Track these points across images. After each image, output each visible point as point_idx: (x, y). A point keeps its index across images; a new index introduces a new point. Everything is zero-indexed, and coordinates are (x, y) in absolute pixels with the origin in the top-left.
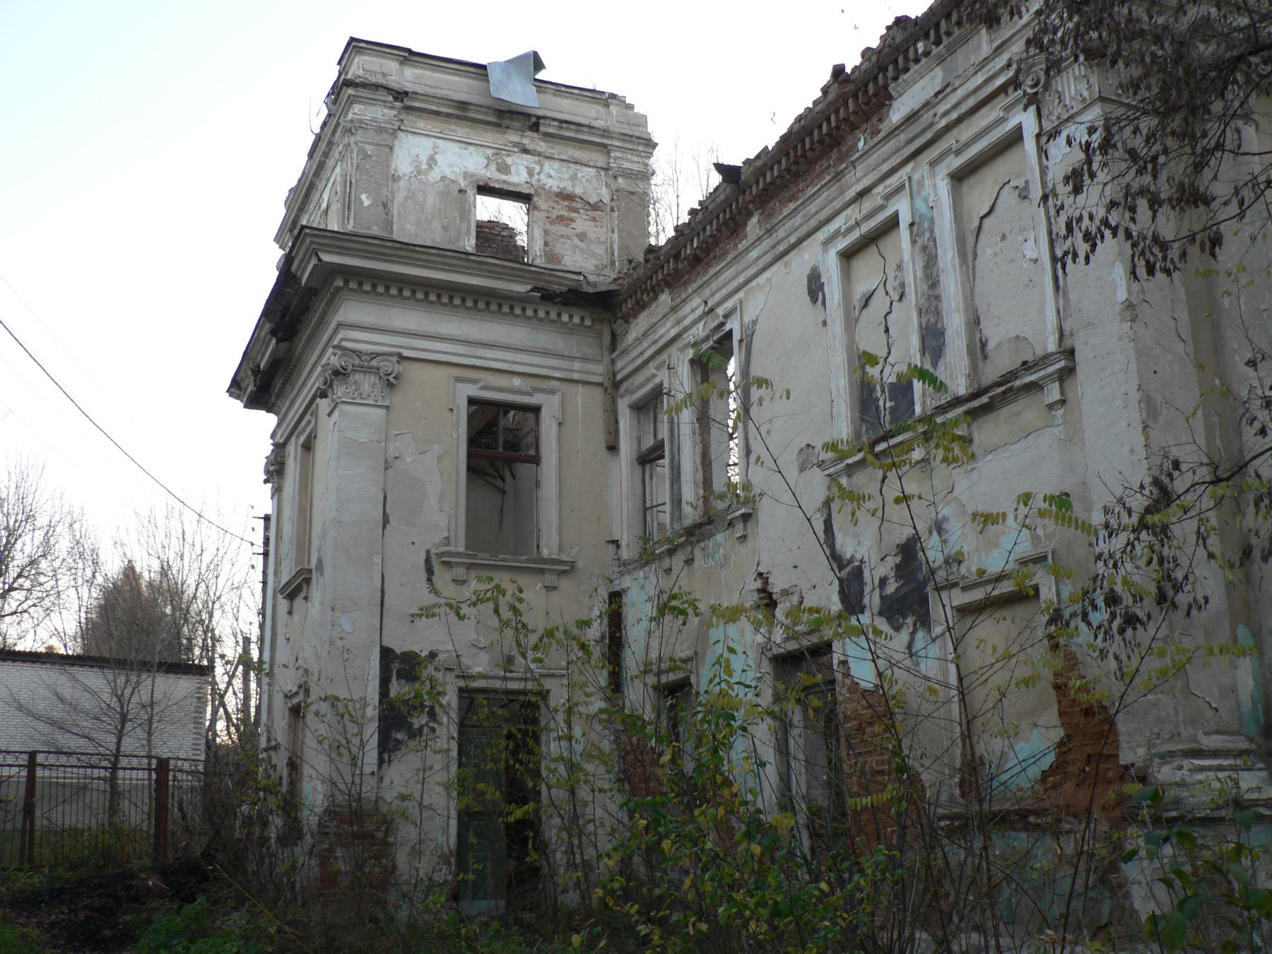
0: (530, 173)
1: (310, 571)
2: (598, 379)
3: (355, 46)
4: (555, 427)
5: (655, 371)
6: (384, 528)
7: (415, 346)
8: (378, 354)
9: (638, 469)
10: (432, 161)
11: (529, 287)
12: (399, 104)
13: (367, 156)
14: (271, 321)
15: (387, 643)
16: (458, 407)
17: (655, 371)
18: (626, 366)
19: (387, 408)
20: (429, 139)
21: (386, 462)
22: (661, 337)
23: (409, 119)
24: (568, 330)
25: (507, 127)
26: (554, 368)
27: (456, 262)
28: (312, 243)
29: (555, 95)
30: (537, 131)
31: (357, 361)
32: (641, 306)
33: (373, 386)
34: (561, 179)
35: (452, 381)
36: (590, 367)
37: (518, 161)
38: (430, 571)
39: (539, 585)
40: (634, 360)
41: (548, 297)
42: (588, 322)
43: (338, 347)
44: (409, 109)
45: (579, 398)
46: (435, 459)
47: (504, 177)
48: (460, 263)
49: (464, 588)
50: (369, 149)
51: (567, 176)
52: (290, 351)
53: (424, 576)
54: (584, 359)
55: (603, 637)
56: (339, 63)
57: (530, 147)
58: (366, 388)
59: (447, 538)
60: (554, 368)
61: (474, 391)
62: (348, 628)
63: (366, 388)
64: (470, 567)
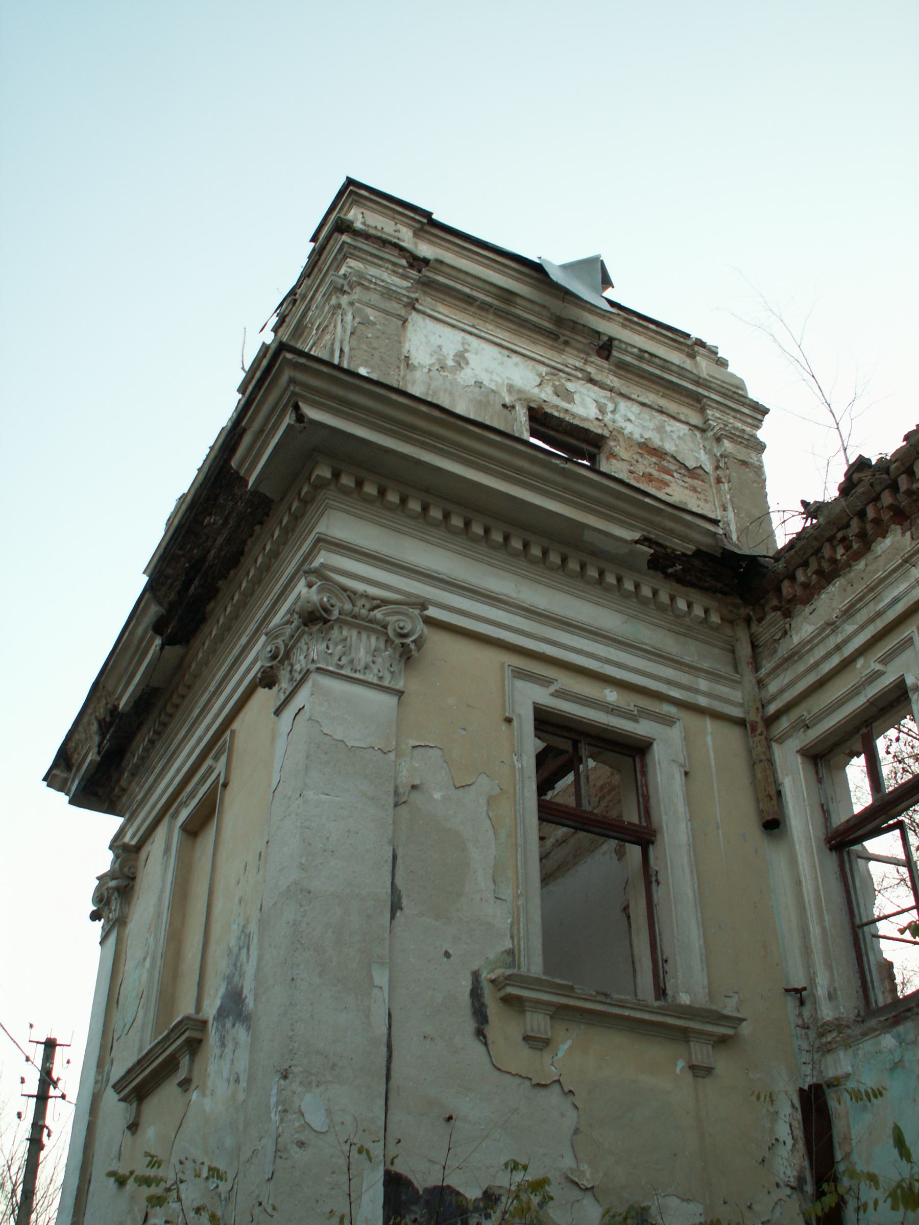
0: (602, 409)
1: (204, 1023)
2: (737, 712)
3: (352, 191)
4: (678, 778)
5: (878, 667)
6: (393, 917)
7: (448, 605)
8: (385, 602)
9: (832, 860)
10: (461, 360)
11: (637, 536)
12: (413, 273)
13: (366, 322)
14: (160, 603)
15: (399, 1167)
16: (520, 716)
17: (878, 667)
18: (782, 691)
19: (400, 693)
20: (457, 332)
21: (396, 793)
22: (895, 601)
23: (426, 302)
24: (683, 627)
25: (566, 343)
26: (669, 682)
27: (525, 465)
28: (292, 381)
29: (624, 326)
30: (607, 358)
31: (348, 606)
32: (810, 593)
33: (375, 652)
34: (644, 427)
35: (508, 673)
36: (723, 690)
37: (584, 390)
38: (480, 1014)
39: (681, 1064)
40: (817, 665)
41: (662, 562)
42: (715, 618)
43: (317, 572)
44: (427, 285)
45: (709, 739)
46: (483, 801)
47: (565, 405)
48: (535, 469)
49: (547, 1056)
50: (372, 315)
51: (651, 425)
52: (180, 667)
53: (470, 1025)
54: (713, 675)
55: (801, 1180)
56: (314, 239)
57: (597, 377)
58: (362, 655)
59: (510, 952)
60: (669, 682)
61: (543, 696)
62: (317, 1120)
63: (362, 655)
64: (560, 1013)
